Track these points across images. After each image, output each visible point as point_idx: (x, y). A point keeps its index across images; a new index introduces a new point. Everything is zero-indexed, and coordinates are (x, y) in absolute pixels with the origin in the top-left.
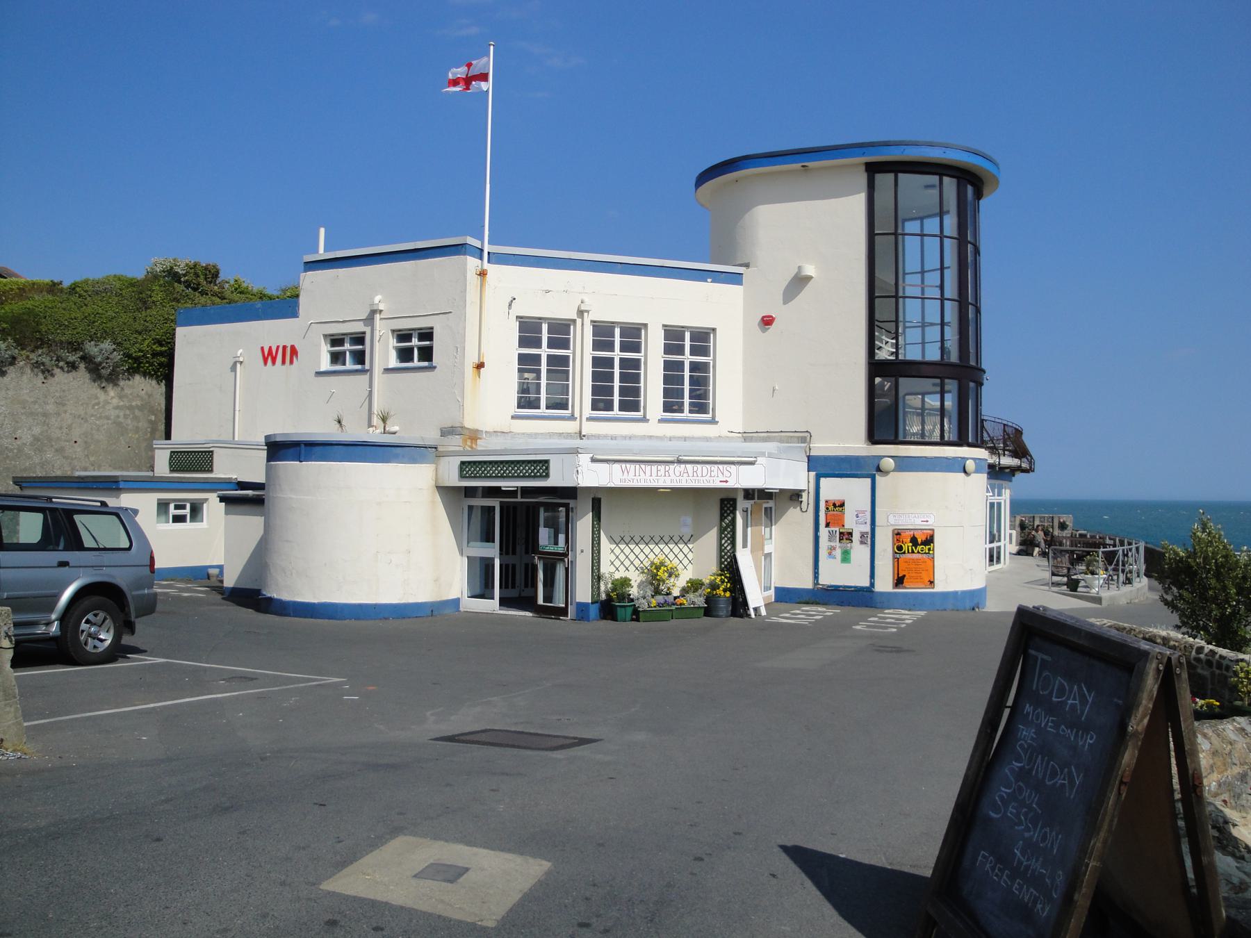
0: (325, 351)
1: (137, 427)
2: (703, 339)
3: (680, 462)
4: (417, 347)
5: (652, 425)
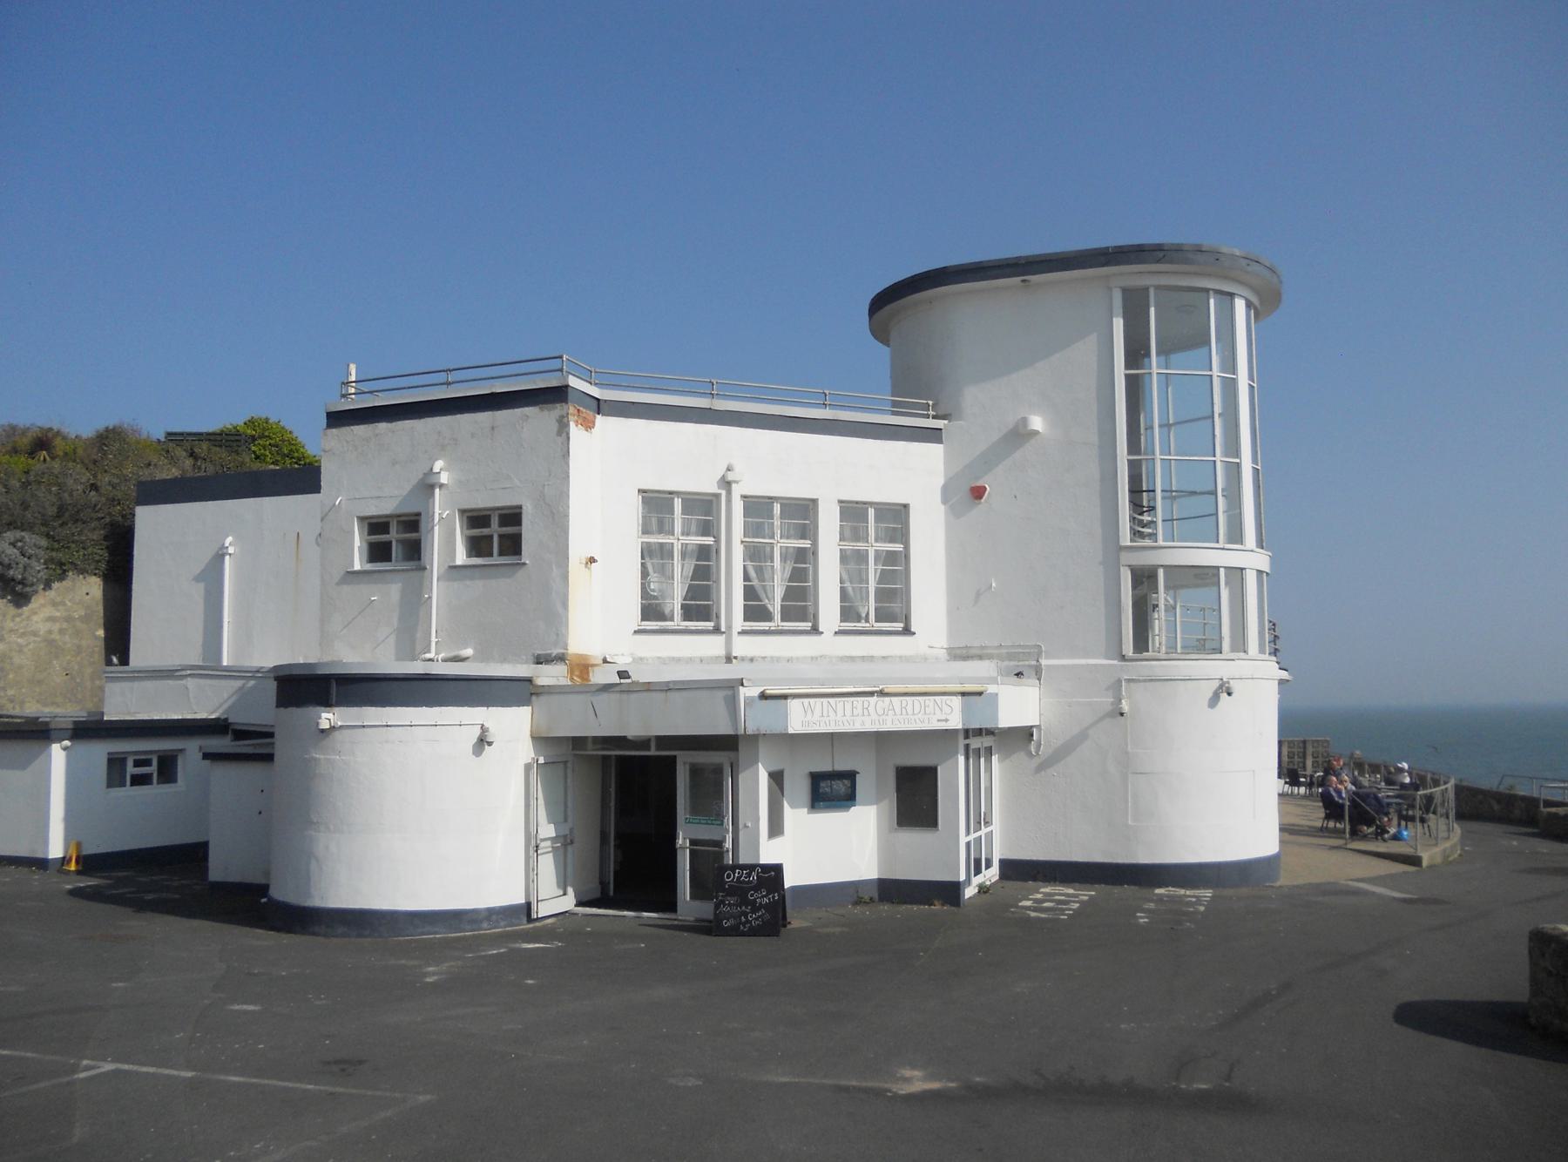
0: (358, 541)
1: (79, 647)
2: (896, 518)
3: (882, 693)
4: (498, 534)
5: (826, 648)
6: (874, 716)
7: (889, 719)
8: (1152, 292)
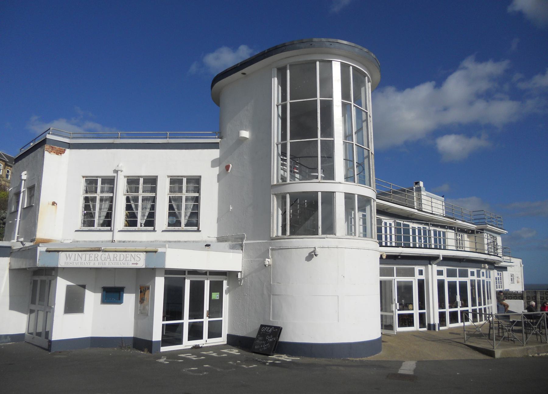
2: (195, 182)
6: (100, 261)
7: (107, 262)
8: (318, 63)
